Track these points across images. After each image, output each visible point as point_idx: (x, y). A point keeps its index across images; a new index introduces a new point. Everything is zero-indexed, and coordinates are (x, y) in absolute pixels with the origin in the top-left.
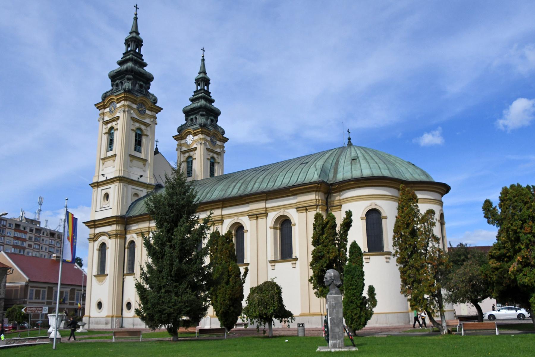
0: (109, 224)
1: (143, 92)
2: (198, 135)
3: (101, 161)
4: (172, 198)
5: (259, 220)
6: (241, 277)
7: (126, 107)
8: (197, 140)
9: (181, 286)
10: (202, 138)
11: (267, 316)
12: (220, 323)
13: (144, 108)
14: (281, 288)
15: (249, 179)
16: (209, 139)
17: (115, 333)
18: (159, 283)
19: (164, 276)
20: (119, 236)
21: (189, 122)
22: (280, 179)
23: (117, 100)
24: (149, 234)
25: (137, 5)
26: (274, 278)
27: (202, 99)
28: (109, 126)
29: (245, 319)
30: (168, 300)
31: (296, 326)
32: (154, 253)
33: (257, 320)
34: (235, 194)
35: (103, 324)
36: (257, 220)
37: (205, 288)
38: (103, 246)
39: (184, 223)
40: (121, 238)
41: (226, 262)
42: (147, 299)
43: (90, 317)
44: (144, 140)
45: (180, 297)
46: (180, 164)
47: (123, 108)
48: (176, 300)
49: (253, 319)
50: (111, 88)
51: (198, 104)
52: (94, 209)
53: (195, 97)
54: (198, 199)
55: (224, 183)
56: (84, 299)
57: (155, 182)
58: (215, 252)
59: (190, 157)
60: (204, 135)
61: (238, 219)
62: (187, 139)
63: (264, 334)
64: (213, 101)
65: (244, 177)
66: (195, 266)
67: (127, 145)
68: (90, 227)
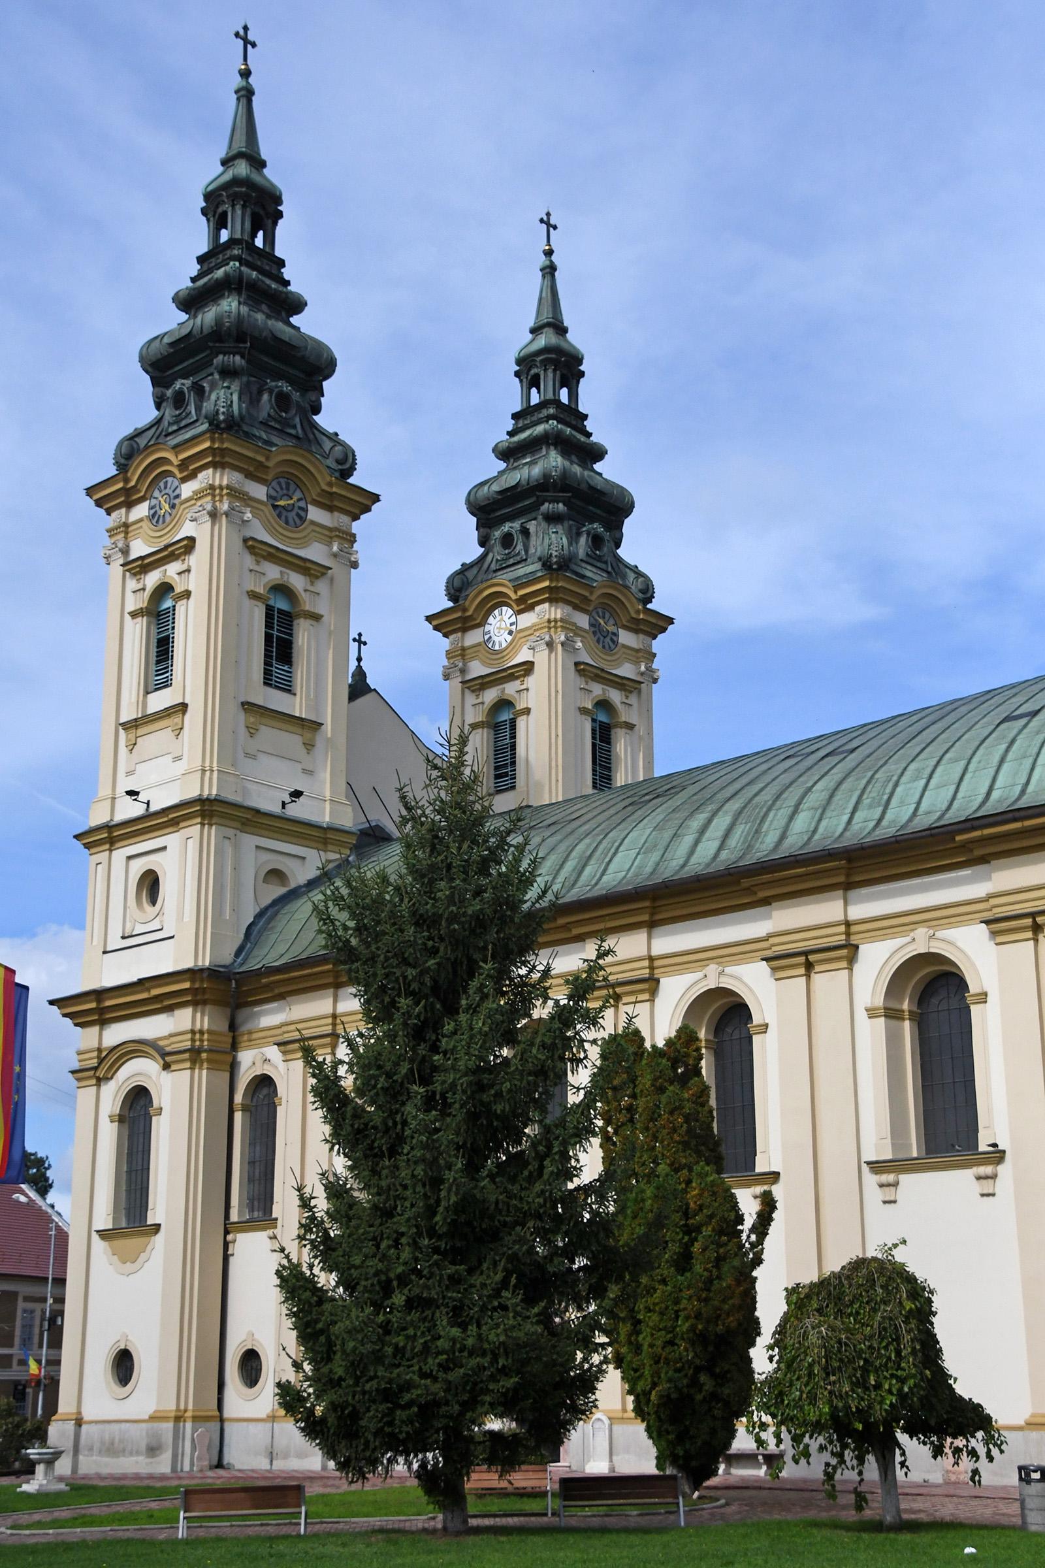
0: (165, 1005)
1: (294, 427)
2: (537, 609)
3: (122, 732)
4: (430, 891)
5: (818, 979)
6: (744, 1237)
7: (221, 496)
8: (534, 628)
9: (477, 1280)
10: (556, 621)
11: (867, 1425)
12: (653, 1451)
13: (298, 495)
14: (931, 1292)
15: (767, 796)
16: (583, 621)
17: (190, 1496)
18: (380, 1266)
19: (403, 1234)
20: (204, 1055)
21: (498, 552)
22: (908, 791)
23: (183, 465)
24: (334, 1047)
25: (246, 28)
26: (895, 1246)
27: (548, 445)
28: (152, 579)
29: (768, 1436)
30: (422, 1341)
31: (1014, 1479)
32: (359, 1131)
33: (821, 1440)
34: (708, 865)
35: (138, 1453)
36: (808, 976)
37: (582, 1288)
38: (138, 1100)
39: (484, 997)
40: (214, 1066)
41: (676, 1168)
42: (328, 1339)
43: (79, 1422)
44: (304, 636)
45: (473, 1329)
46: (463, 741)
47: (207, 503)
48: (454, 1340)
49: (803, 1435)
50: (154, 414)
51: (531, 470)
52: (97, 941)
53: (516, 439)
54: (545, 892)
55: (658, 815)
56: (56, 1342)
57: (355, 817)
58: (623, 1124)
59: (504, 704)
60: (560, 604)
61: (722, 973)
62: (487, 628)
63: (859, 1508)
64: (598, 454)
65: (742, 788)
66: (538, 1187)
67: (231, 662)
68: (80, 1020)
